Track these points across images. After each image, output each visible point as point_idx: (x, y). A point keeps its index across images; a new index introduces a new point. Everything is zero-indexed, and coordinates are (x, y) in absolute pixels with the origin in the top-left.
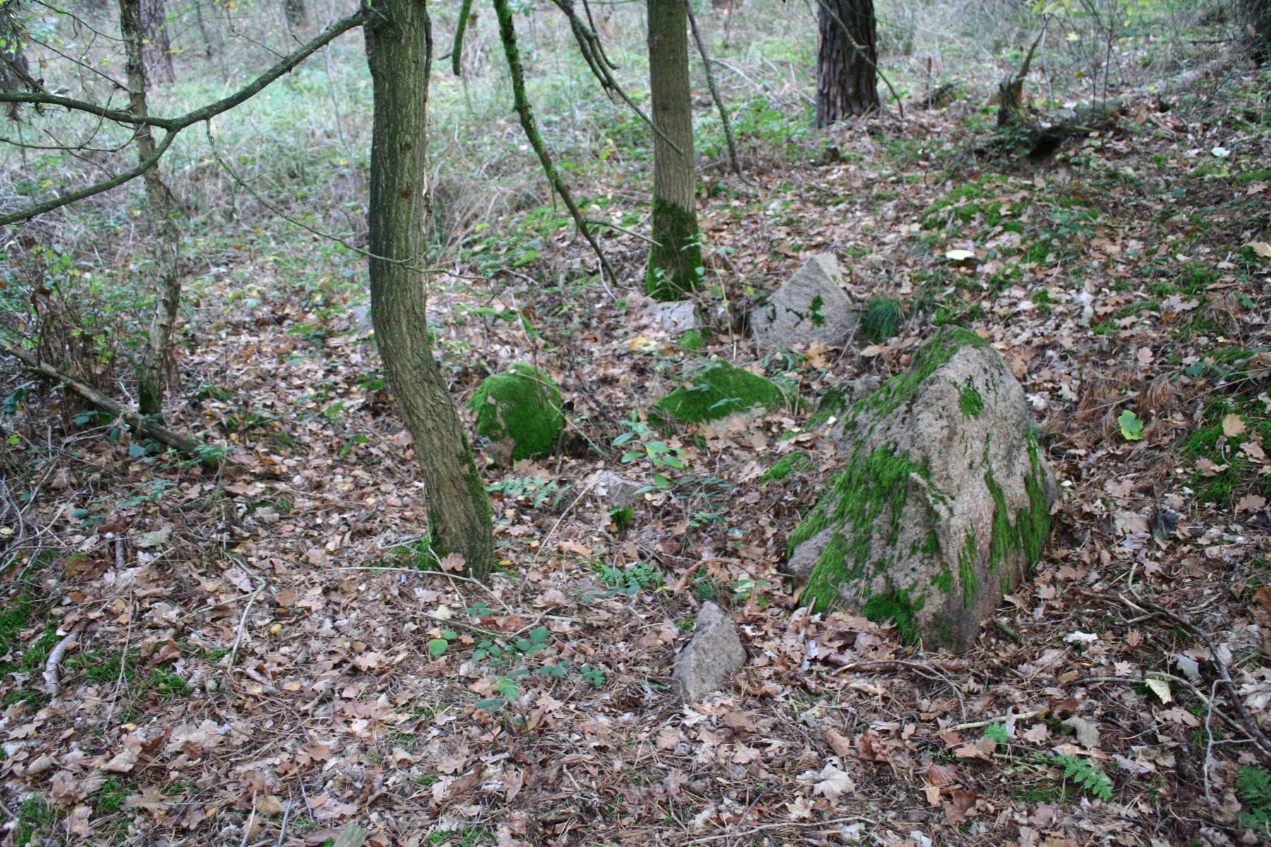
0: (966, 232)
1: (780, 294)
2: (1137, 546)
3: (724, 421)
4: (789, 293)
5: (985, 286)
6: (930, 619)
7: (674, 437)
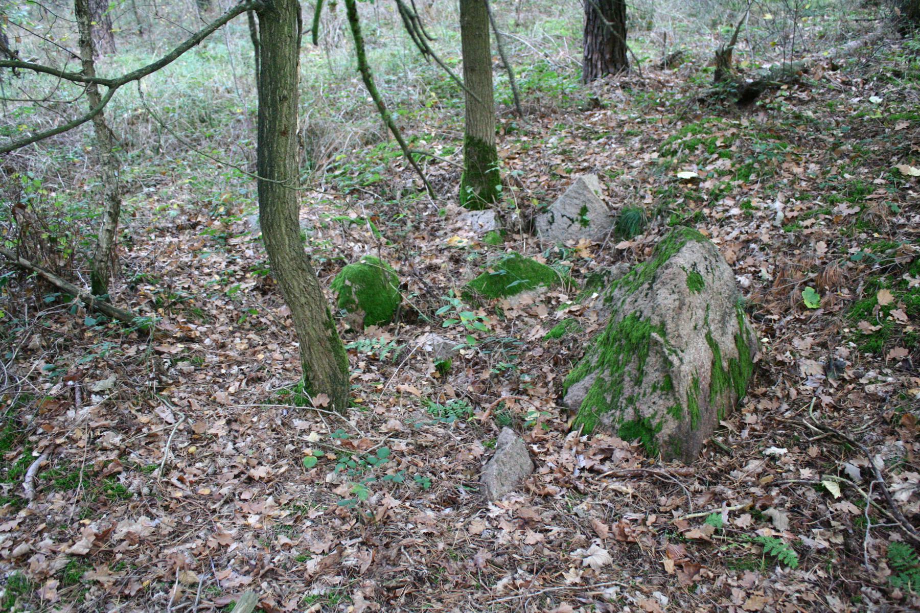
0: (692, 158)
3: (517, 297)
4: (563, 203)
5: (706, 197)
6: (666, 438)
7: (481, 309)
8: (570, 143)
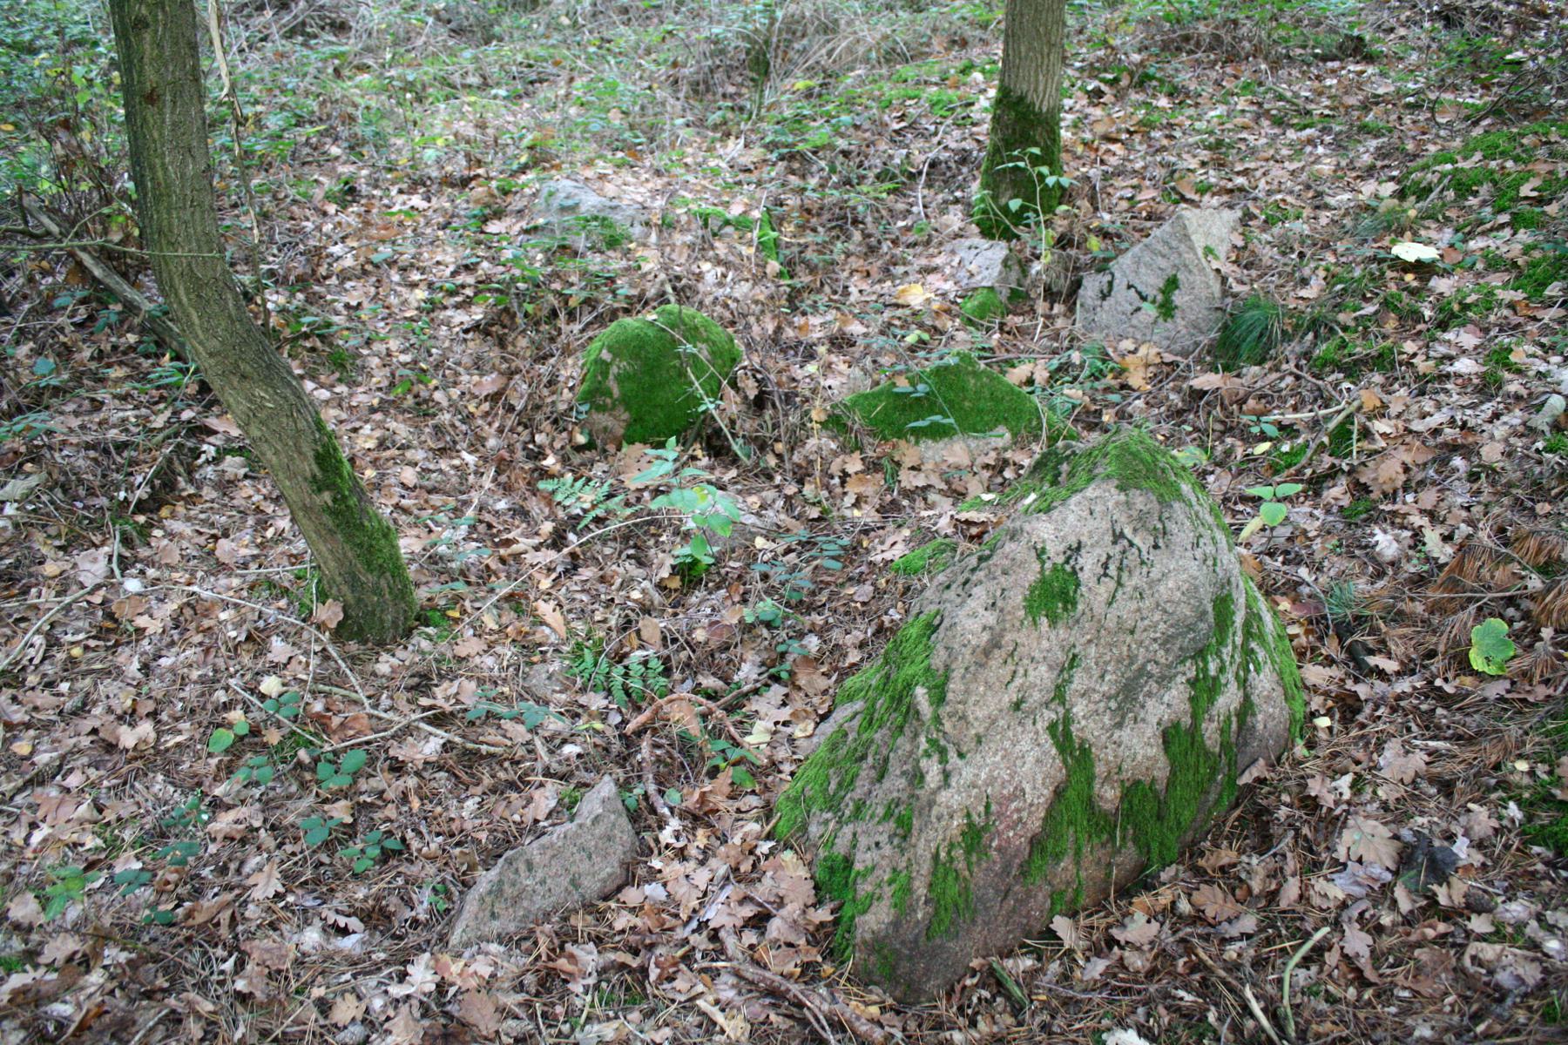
0: (1452, 214)
1: (1126, 260)
2: (1357, 891)
3: (941, 444)
4: (1138, 261)
5: (1427, 313)
6: (868, 936)
7: (857, 455)
8: (1244, 128)
